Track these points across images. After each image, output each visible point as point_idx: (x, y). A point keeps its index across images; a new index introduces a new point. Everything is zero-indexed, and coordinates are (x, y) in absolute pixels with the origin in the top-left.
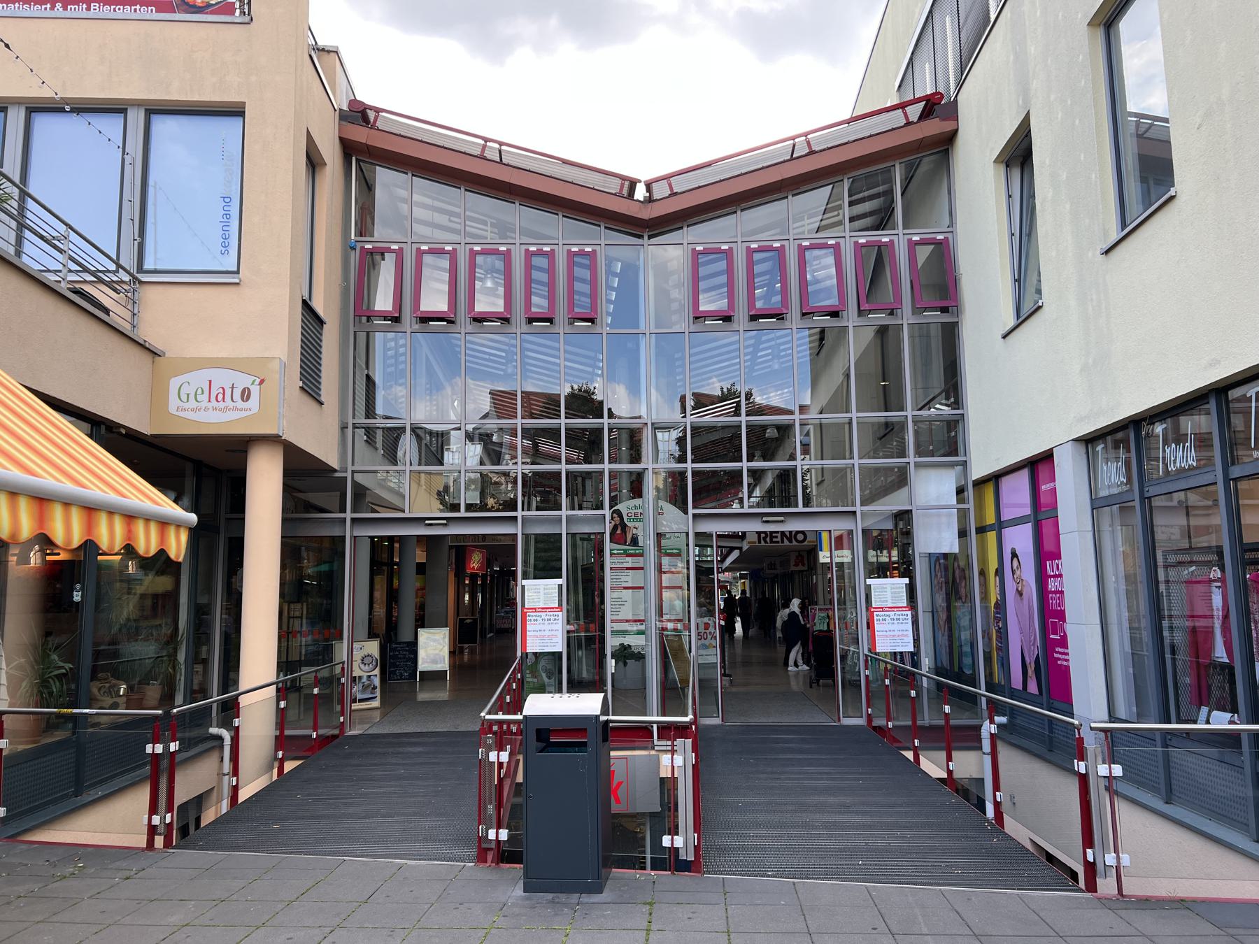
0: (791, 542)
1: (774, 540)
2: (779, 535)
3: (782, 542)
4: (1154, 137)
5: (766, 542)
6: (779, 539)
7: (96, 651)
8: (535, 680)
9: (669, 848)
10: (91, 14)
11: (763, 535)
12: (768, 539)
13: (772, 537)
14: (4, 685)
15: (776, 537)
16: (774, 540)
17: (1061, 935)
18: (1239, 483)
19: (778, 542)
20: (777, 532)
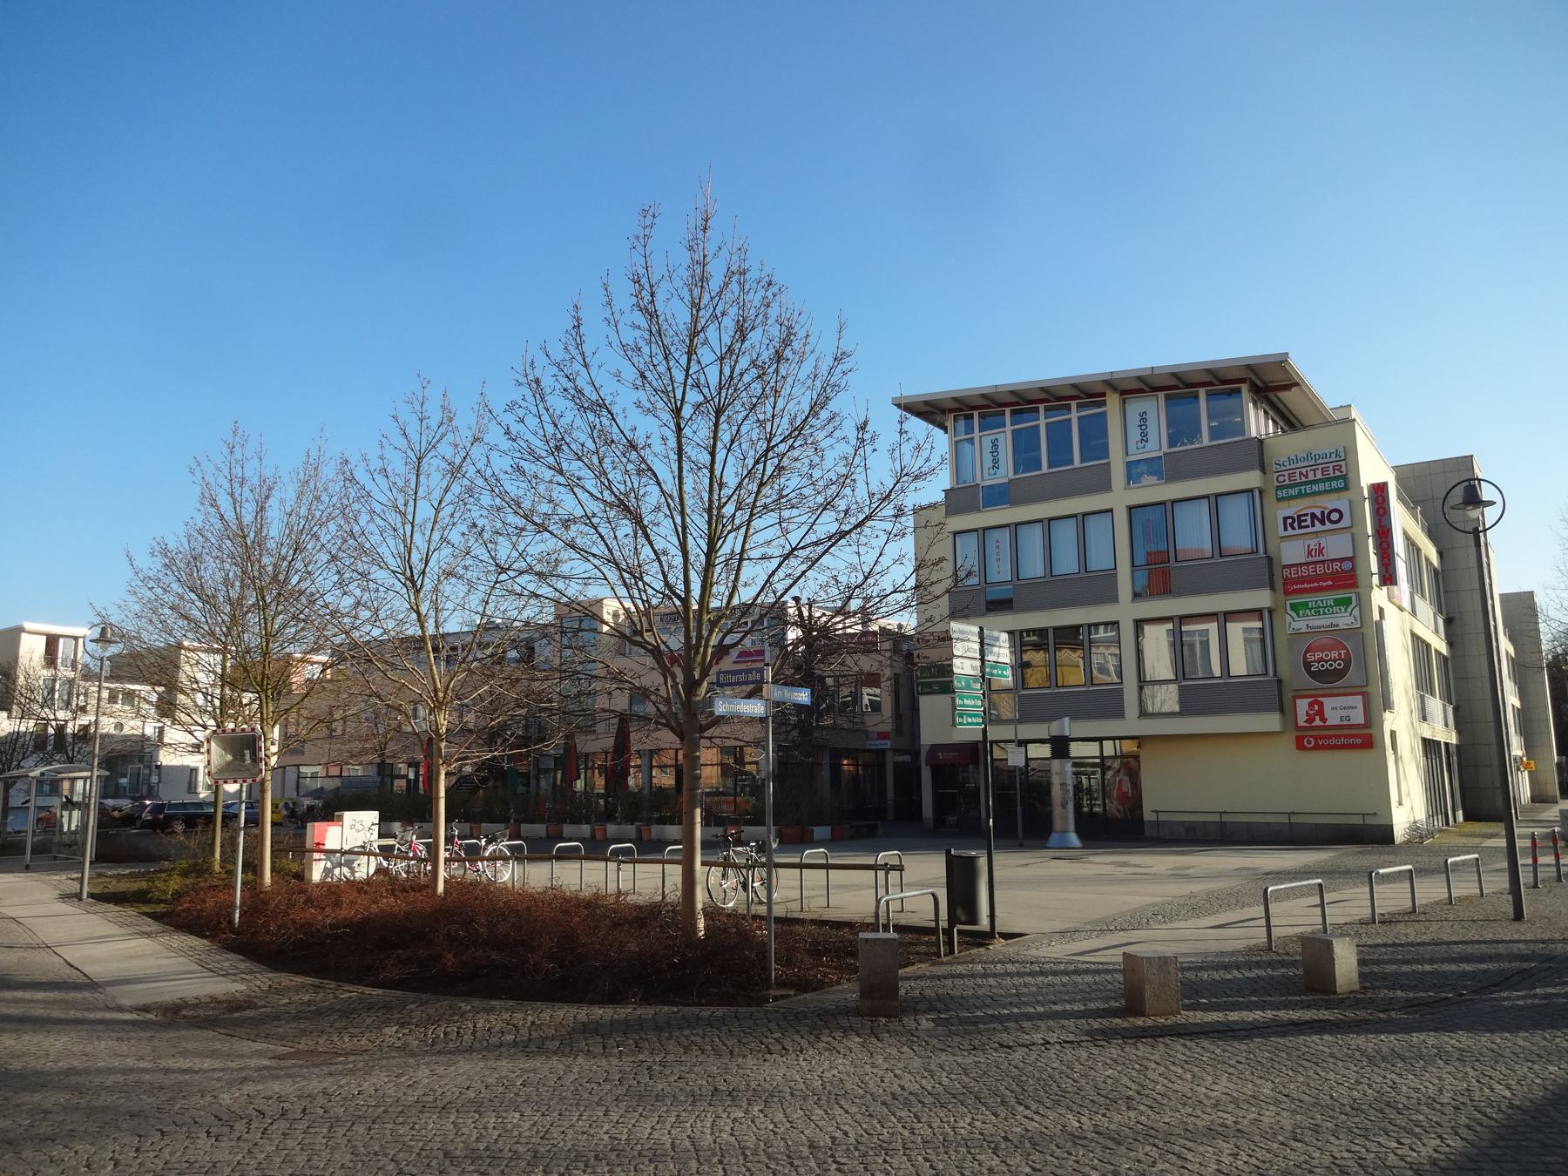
0: (1323, 524)
1: (1303, 524)
2: (1309, 518)
3: (1313, 525)
4: (1282, 399)
5: (1294, 528)
6: (1309, 523)
7: (210, 819)
8: (487, 854)
9: (1020, 769)
10: (1120, 951)
11: (1289, 521)
12: (1296, 525)
13: (1300, 521)
14: (1057, 774)
15: (1306, 520)
16: (1303, 524)
17: (605, 582)
18: (1150, 710)
19: (1308, 526)
20: (1307, 515)
